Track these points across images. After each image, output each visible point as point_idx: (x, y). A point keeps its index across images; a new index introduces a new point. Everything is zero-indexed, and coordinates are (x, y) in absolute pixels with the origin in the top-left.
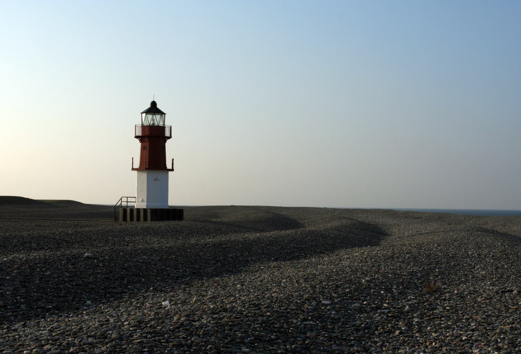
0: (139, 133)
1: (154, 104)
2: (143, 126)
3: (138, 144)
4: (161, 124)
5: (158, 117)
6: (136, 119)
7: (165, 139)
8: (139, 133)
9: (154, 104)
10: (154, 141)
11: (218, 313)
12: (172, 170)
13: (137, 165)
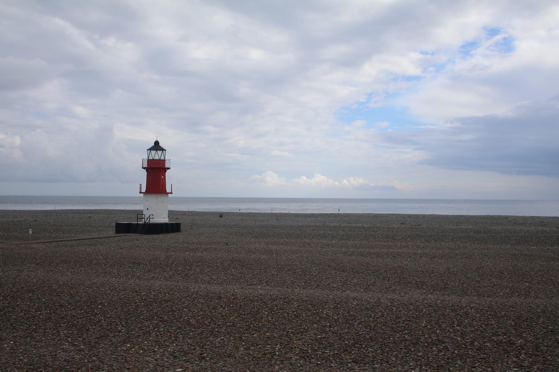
0: (146, 166)
1: (157, 143)
2: (149, 161)
3: (144, 173)
4: (162, 158)
5: (160, 152)
6: (141, 157)
7: (165, 169)
8: (146, 166)
9: (157, 143)
10: (156, 174)
11: (221, 284)
12: (171, 193)
13: (144, 190)
